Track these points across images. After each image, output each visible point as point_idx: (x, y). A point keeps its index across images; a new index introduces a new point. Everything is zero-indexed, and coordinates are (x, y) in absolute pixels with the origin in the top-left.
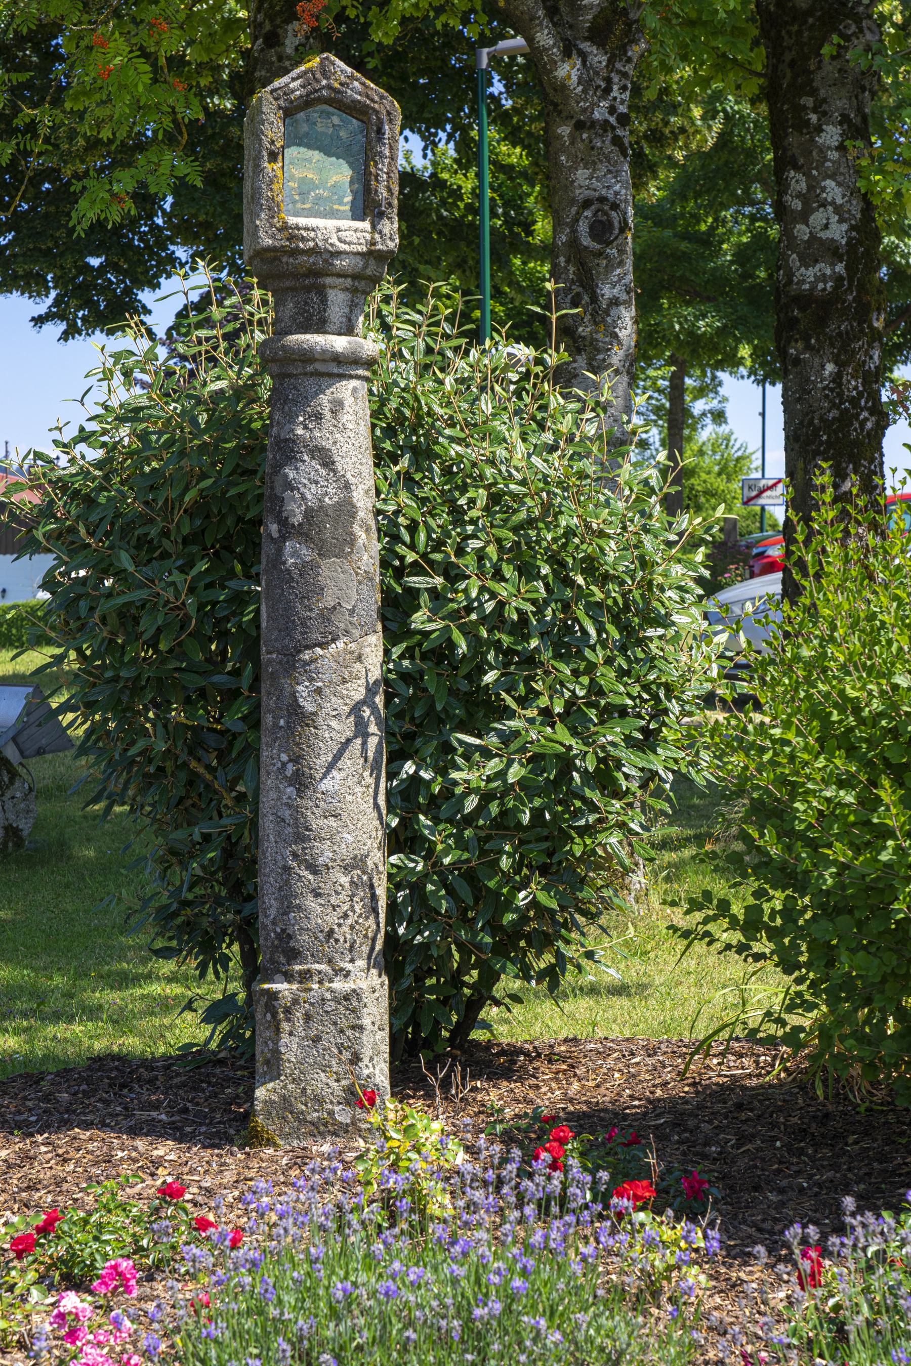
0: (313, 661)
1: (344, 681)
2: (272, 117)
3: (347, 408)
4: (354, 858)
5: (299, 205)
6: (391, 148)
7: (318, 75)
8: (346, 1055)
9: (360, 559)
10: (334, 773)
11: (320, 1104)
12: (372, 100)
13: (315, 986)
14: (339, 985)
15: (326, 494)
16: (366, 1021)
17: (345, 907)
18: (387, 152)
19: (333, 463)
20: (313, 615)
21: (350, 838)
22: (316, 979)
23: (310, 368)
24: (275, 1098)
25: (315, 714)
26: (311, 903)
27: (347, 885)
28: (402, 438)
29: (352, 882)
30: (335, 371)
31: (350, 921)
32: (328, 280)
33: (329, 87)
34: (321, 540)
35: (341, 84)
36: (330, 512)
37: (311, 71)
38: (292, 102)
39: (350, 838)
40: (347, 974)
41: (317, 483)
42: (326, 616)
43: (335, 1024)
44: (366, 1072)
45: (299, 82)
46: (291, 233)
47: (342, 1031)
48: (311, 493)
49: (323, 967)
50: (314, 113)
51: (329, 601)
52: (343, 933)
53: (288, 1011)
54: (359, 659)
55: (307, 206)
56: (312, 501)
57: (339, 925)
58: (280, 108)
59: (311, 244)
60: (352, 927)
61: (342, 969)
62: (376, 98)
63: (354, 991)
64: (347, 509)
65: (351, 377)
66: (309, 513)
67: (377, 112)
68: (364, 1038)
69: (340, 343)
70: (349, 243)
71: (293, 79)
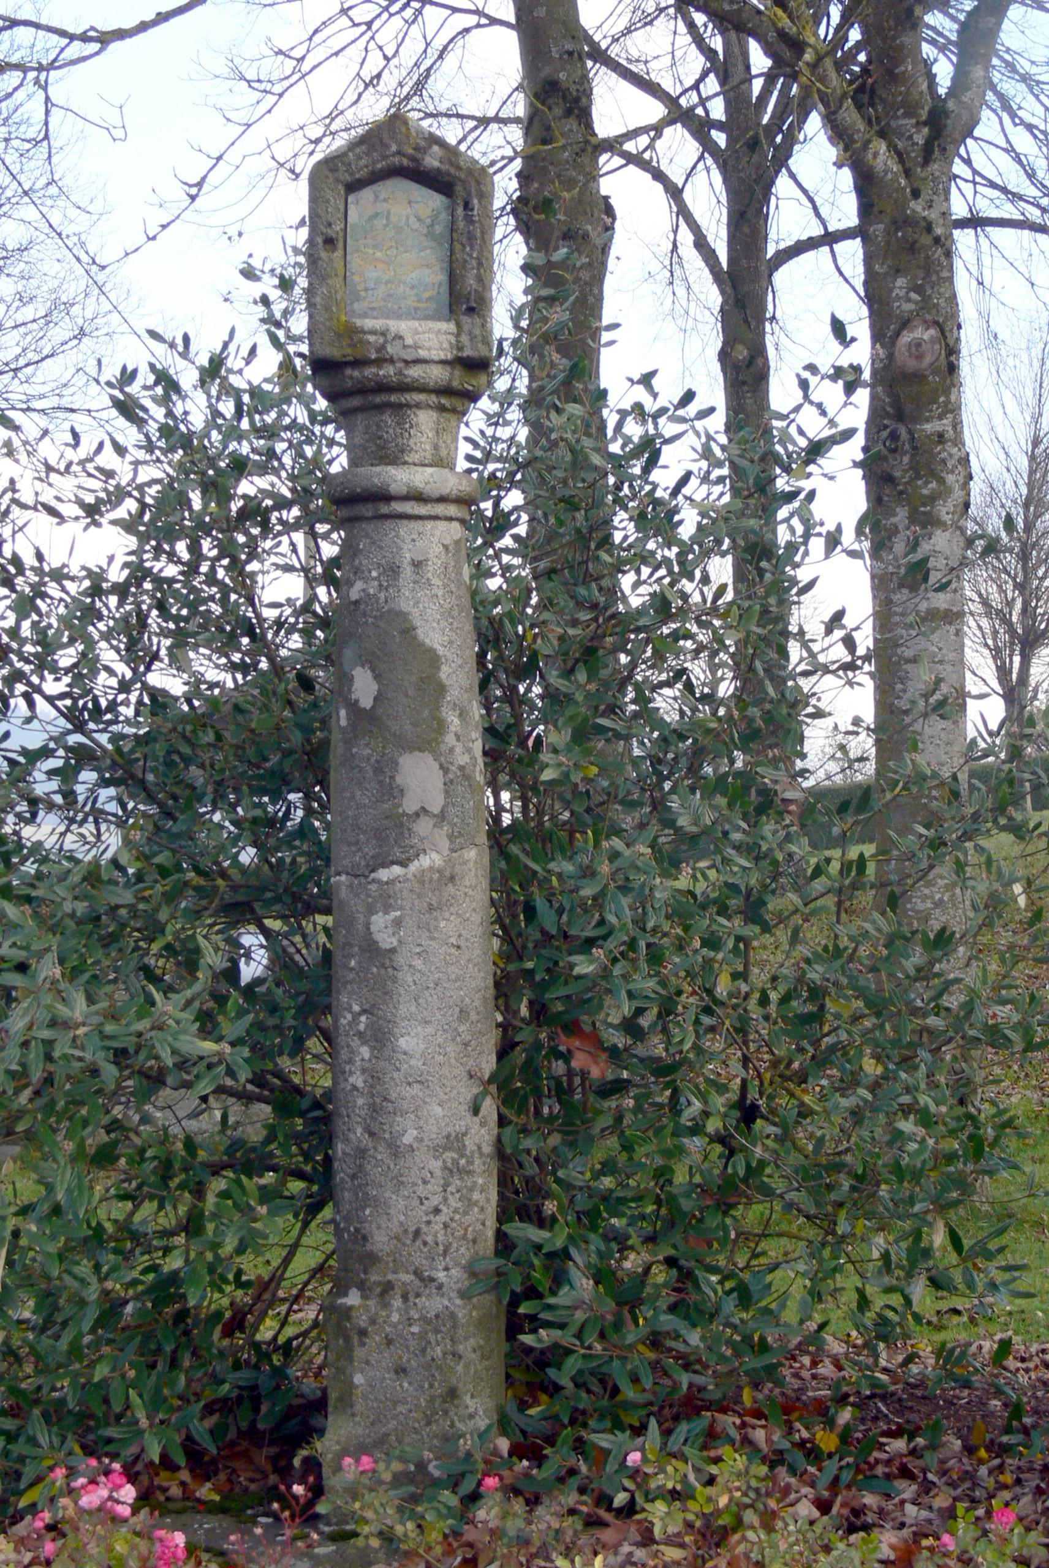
4: (448, 1137)
17: (436, 1200)
25: (393, 951)
27: (438, 1172)
29: (445, 1168)
31: (442, 1218)
49: (408, 1278)
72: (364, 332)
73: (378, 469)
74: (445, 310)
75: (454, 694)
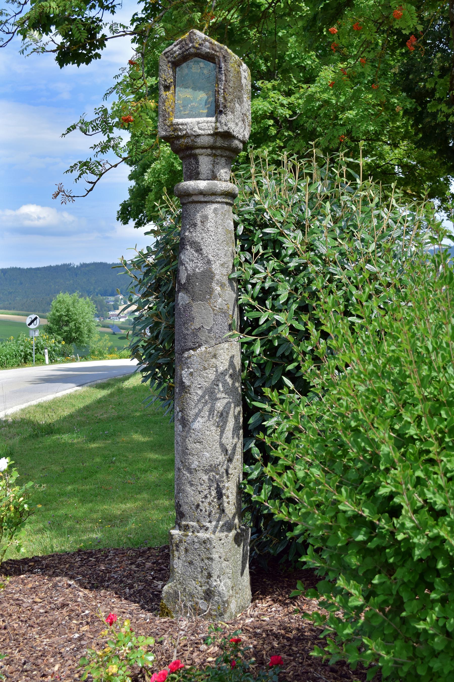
0: (190, 357)
1: (205, 369)
2: (165, 67)
3: (210, 219)
4: (211, 466)
5: (183, 113)
6: (226, 75)
7: (188, 42)
8: (205, 573)
9: (216, 302)
10: (199, 419)
11: (192, 598)
12: (215, 51)
13: (190, 534)
14: (202, 535)
15: (197, 266)
16: (215, 556)
17: (206, 492)
18: (224, 78)
19: (201, 250)
20: (189, 332)
21: (208, 455)
22: (191, 530)
23: (190, 199)
24: (171, 591)
25: (189, 386)
26: (189, 489)
27: (207, 480)
28: (252, 235)
29: (209, 479)
30: (203, 199)
31: (208, 500)
32: (197, 151)
33: (194, 47)
34: (193, 292)
35: (200, 45)
36: (198, 277)
37: (185, 40)
38: (175, 58)
39: (208, 455)
40: (207, 529)
41: (193, 261)
42: (195, 333)
43: (199, 555)
44: (215, 584)
45: (178, 47)
46: (175, 127)
47: (203, 560)
48: (190, 266)
49: (195, 524)
50: (191, 63)
51: (197, 325)
52: (205, 506)
53: (177, 546)
54: (215, 356)
55: (187, 112)
56: (190, 272)
57: (202, 502)
58: (169, 62)
59: (184, 132)
60: (210, 504)
61: (204, 526)
62: (218, 50)
63: (208, 539)
64: (208, 275)
65: (213, 202)
66: (189, 278)
67: (218, 57)
68: (213, 565)
69: (202, 184)
70: (204, 130)
71: (175, 46)
72: (178, 125)
73: (187, 182)
74: (213, 112)
75: (123, 506)
